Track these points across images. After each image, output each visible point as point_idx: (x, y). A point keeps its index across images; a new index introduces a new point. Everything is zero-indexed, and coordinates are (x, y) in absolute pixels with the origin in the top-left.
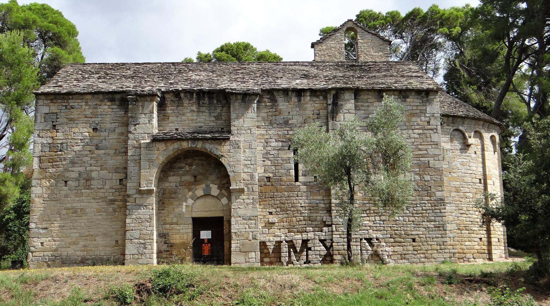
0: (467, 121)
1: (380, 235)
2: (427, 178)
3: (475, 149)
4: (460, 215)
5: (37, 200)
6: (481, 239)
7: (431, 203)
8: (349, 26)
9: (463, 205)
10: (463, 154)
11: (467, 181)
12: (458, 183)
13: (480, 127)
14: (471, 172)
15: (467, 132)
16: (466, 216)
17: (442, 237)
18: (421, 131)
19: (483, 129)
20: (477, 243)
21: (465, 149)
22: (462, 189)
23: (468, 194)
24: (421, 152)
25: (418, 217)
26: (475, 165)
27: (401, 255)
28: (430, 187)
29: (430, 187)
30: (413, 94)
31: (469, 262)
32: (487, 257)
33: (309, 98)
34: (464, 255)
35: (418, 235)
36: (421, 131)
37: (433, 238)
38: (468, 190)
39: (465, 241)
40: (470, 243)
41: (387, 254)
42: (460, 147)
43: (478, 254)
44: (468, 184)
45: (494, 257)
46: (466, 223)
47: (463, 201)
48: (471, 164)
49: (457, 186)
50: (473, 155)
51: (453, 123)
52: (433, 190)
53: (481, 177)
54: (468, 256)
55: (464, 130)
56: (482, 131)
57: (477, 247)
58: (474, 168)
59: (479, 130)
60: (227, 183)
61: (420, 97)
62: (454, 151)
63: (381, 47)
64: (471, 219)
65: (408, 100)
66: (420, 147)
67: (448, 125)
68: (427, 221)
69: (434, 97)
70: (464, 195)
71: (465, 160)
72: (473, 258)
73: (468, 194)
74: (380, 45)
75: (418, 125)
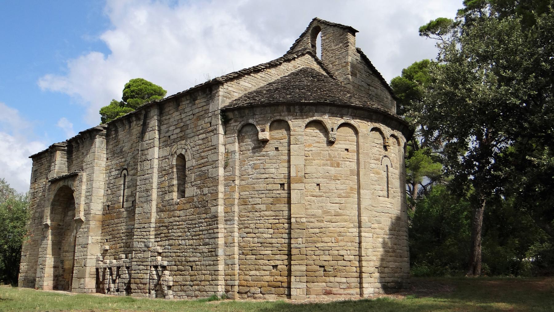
0: (258, 111)
1: (165, 263)
2: (206, 190)
3: (277, 145)
4: (245, 235)
5: (394, 181)
6: (275, 267)
7: (206, 222)
8: (314, 26)
9: (250, 222)
10: (257, 154)
11: (258, 189)
12: (247, 193)
13: (283, 114)
14: (267, 176)
15: (259, 124)
16: (254, 235)
17: (214, 265)
18: (204, 136)
19: (288, 115)
20: (268, 273)
21: (260, 147)
22: (250, 200)
23: (258, 207)
24: (203, 161)
25: (196, 239)
26: (275, 165)
27: (181, 285)
28: (207, 201)
29: (207, 201)
30: (200, 94)
31: (255, 298)
32: (286, 293)
33: (135, 122)
34: (248, 289)
35: (194, 261)
36: (204, 136)
37: (206, 266)
38: (259, 201)
39: (251, 270)
40: (257, 273)
41: (166, 284)
42: (253, 145)
43: (269, 288)
44: (260, 192)
45: (293, 292)
46: (252, 245)
47: (251, 215)
48: (267, 166)
49: (245, 197)
50: (272, 153)
51: (242, 117)
52: (209, 205)
53: (285, 181)
54: (253, 290)
55: (255, 123)
56: (286, 119)
57: (268, 278)
58: (273, 170)
59: (282, 118)
60: (133, 206)
61: (205, 95)
62: (245, 152)
63: (342, 37)
64: (260, 240)
65: (197, 102)
66: (203, 154)
67: (235, 121)
68: (203, 245)
69: (216, 91)
70: (253, 208)
71: (258, 162)
72: (261, 292)
73: (258, 207)
74: (341, 35)
75: (202, 129)
